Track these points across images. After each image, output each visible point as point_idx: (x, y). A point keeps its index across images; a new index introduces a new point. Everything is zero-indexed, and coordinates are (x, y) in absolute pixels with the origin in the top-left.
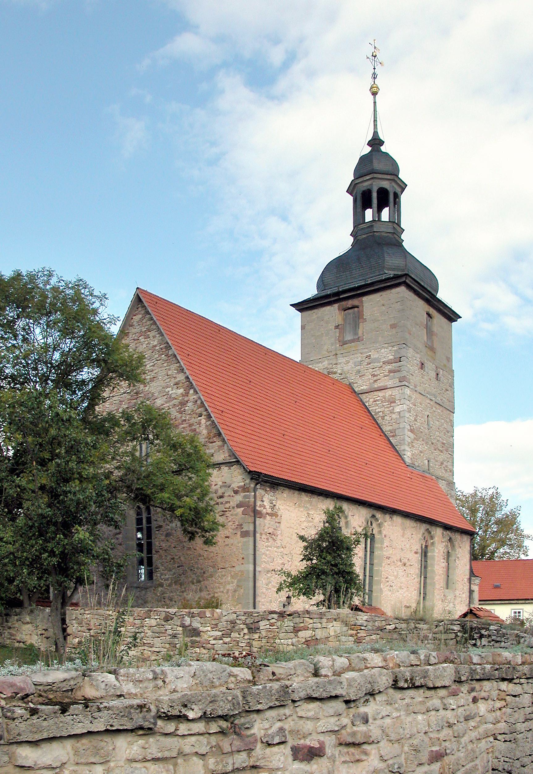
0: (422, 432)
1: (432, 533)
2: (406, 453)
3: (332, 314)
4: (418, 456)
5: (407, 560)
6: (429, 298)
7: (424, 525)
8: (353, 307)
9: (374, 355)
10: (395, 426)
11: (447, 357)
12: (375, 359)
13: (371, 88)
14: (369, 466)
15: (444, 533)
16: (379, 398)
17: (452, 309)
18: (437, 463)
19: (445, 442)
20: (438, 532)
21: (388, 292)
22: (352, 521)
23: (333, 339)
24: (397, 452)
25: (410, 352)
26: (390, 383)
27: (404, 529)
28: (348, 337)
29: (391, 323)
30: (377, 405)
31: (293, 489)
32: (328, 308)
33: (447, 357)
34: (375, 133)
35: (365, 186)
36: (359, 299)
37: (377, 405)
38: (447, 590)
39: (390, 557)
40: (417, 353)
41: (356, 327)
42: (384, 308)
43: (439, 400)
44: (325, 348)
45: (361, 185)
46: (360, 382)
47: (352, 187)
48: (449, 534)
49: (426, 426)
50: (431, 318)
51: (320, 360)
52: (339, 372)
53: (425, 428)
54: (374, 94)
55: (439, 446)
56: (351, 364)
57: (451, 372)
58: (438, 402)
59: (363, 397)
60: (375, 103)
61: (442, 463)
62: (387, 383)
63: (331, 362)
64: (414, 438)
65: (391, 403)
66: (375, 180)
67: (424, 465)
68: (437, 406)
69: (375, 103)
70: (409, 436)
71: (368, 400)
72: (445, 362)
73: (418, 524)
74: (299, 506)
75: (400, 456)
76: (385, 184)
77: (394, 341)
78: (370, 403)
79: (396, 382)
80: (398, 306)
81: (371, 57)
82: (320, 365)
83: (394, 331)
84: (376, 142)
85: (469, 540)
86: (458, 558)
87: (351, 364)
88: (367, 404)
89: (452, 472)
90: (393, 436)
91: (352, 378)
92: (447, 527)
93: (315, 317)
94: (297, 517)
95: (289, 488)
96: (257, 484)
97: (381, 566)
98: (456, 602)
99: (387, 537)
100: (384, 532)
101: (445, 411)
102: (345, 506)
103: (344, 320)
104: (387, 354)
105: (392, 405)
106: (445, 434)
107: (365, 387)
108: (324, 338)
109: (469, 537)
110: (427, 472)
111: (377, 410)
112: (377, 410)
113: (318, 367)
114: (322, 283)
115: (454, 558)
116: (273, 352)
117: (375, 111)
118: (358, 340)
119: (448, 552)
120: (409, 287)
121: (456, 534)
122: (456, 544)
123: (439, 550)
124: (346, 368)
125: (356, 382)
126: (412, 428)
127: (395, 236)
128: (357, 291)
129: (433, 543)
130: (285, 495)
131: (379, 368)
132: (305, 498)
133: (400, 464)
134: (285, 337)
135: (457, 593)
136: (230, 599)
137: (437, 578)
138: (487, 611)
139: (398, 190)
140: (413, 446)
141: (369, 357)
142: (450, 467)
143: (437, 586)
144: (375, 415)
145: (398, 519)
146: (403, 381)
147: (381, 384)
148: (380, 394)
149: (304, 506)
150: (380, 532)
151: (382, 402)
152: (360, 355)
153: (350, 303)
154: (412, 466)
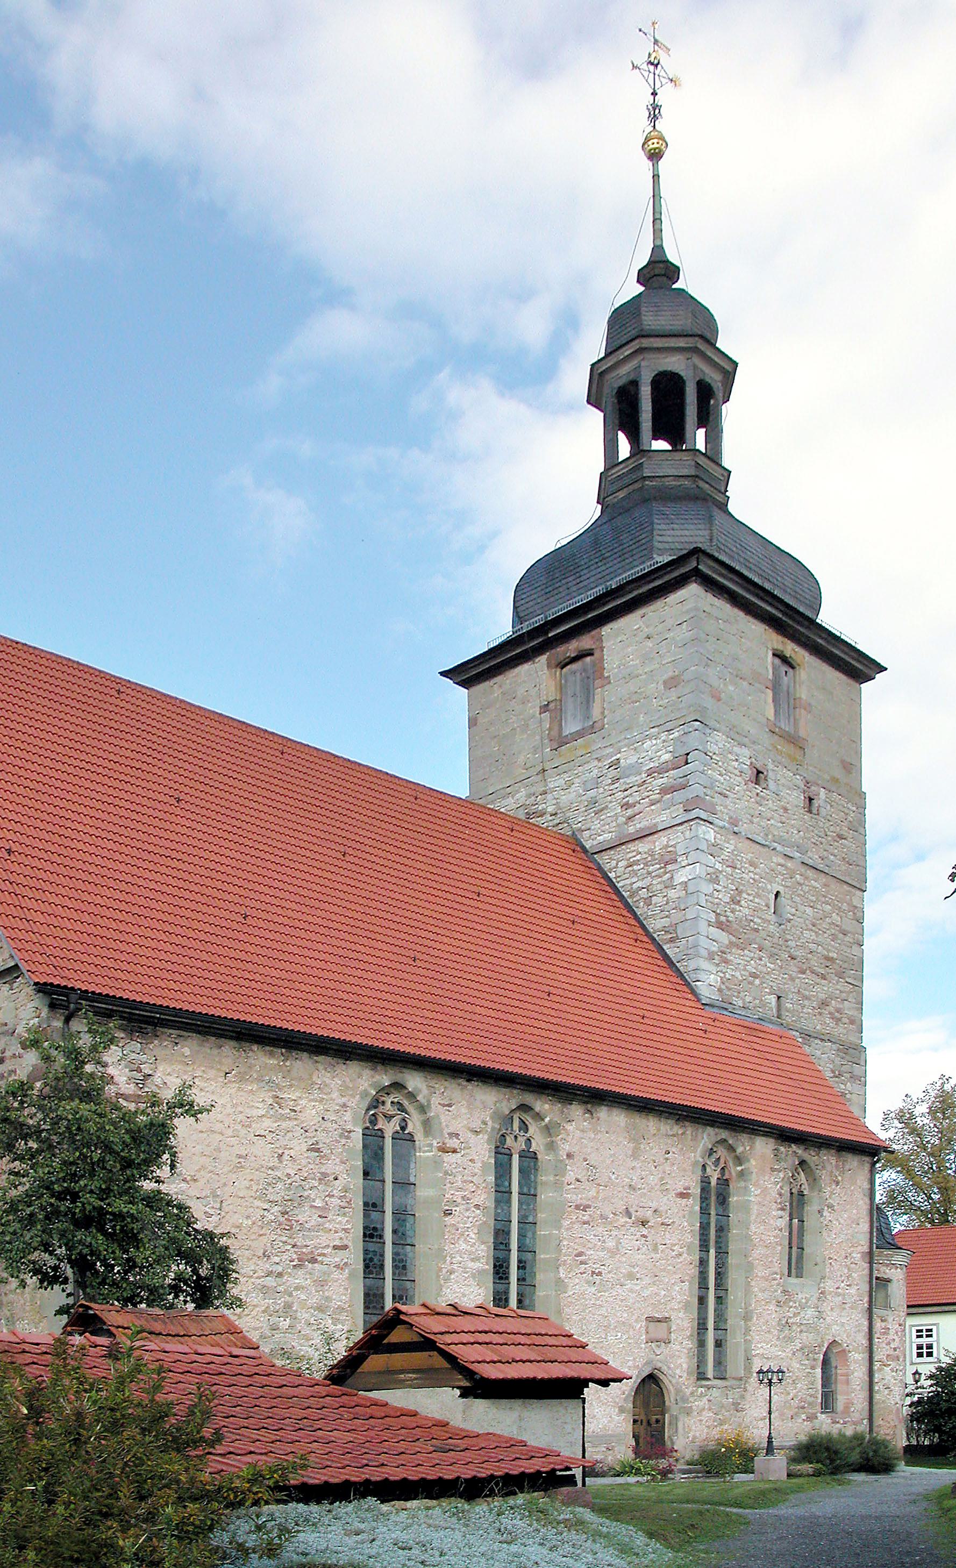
0: (757, 930)
1: (740, 1150)
2: (702, 976)
3: (535, 678)
4: (744, 984)
5: (650, 1213)
6: (774, 611)
7: (709, 1130)
10: (676, 916)
11: (843, 762)
12: (631, 766)
13: (647, 140)
14: (558, 999)
15: (782, 1149)
16: (638, 857)
17: (858, 647)
18: (806, 1003)
20: (761, 1149)
21: (659, 604)
22: (443, 1119)
23: (538, 737)
24: (681, 975)
25: (718, 742)
26: (663, 818)
27: (637, 1139)
28: (571, 727)
29: (665, 677)
30: (635, 873)
31: (214, 1035)
32: (524, 669)
33: (843, 762)
34: (658, 249)
35: (623, 373)
36: (593, 633)
37: (635, 873)
38: (793, 1280)
39: (589, 1207)
40: (741, 744)
41: (588, 702)
42: (649, 644)
43: (813, 857)
44: (521, 759)
45: (614, 374)
46: (596, 825)
47: (594, 386)
48: (800, 1152)
49: (773, 918)
50: (793, 667)
52: (550, 809)
54: (655, 156)
55: (813, 963)
56: (577, 788)
57: (859, 798)
58: (810, 862)
59: (603, 859)
60: (656, 177)
62: (657, 820)
63: (533, 790)
64: (731, 943)
65: (667, 863)
66: (646, 355)
67: (763, 1005)
68: (810, 873)
69: (656, 177)
70: (709, 937)
71: (614, 864)
72: (838, 773)
73: (690, 1129)
74: (242, 1078)
75: (687, 984)
76: (675, 363)
77: (673, 716)
78: (620, 870)
79: (678, 814)
80: (683, 633)
81: (645, 66)
82: (510, 800)
83: (673, 694)
84: (659, 273)
85: (867, 1167)
86: (830, 1206)
87: (577, 788)
88: (612, 875)
90: (672, 940)
91: (578, 820)
92: (786, 1136)
93: (497, 692)
94: (234, 1106)
95: (199, 1033)
96: (67, 1020)
97: (559, 1228)
98: (826, 1307)
99: (578, 1158)
100: (564, 1148)
101: (834, 885)
102: (415, 1081)
103: (561, 688)
104: (658, 750)
105: (669, 867)
106: (834, 937)
107: (607, 836)
108: (518, 738)
109: (867, 1159)
110: (771, 1022)
111: (635, 886)
112: (635, 886)
113: (507, 805)
114: (518, 617)
115: (816, 1207)
116: (386, 777)
117: (656, 196)
118: (592, 729)
119: (801, 1194)
120: (709, 584)
121: (823, 1152)
122: (824, 1175)
123: (765, 1191)
124: (565, 799)
125: (588, 826)
126: (723, 919)
127: (701, 484)
128: (586, 613)
129: (741, 1174)
130: (187, 1051)
131: (639, 786)
132: (262, 1059)
133: (688, 1003)
134: (429, 743)
135: (829, 1285)
136: (27, 1308)
137: (757, 1253)
138: (376, 1403)
139: (714, 377)
140: (726, 962)
143: (760, 1271)
144: (631, 896)
145: (614, 1120)
146: (697, 811)
148: (642, 846)
149: (259, 1080)
150: (551, 1147)
151: (646, 864)
152: (596, 763)
153: (573, 647)
154: (725, 1006)
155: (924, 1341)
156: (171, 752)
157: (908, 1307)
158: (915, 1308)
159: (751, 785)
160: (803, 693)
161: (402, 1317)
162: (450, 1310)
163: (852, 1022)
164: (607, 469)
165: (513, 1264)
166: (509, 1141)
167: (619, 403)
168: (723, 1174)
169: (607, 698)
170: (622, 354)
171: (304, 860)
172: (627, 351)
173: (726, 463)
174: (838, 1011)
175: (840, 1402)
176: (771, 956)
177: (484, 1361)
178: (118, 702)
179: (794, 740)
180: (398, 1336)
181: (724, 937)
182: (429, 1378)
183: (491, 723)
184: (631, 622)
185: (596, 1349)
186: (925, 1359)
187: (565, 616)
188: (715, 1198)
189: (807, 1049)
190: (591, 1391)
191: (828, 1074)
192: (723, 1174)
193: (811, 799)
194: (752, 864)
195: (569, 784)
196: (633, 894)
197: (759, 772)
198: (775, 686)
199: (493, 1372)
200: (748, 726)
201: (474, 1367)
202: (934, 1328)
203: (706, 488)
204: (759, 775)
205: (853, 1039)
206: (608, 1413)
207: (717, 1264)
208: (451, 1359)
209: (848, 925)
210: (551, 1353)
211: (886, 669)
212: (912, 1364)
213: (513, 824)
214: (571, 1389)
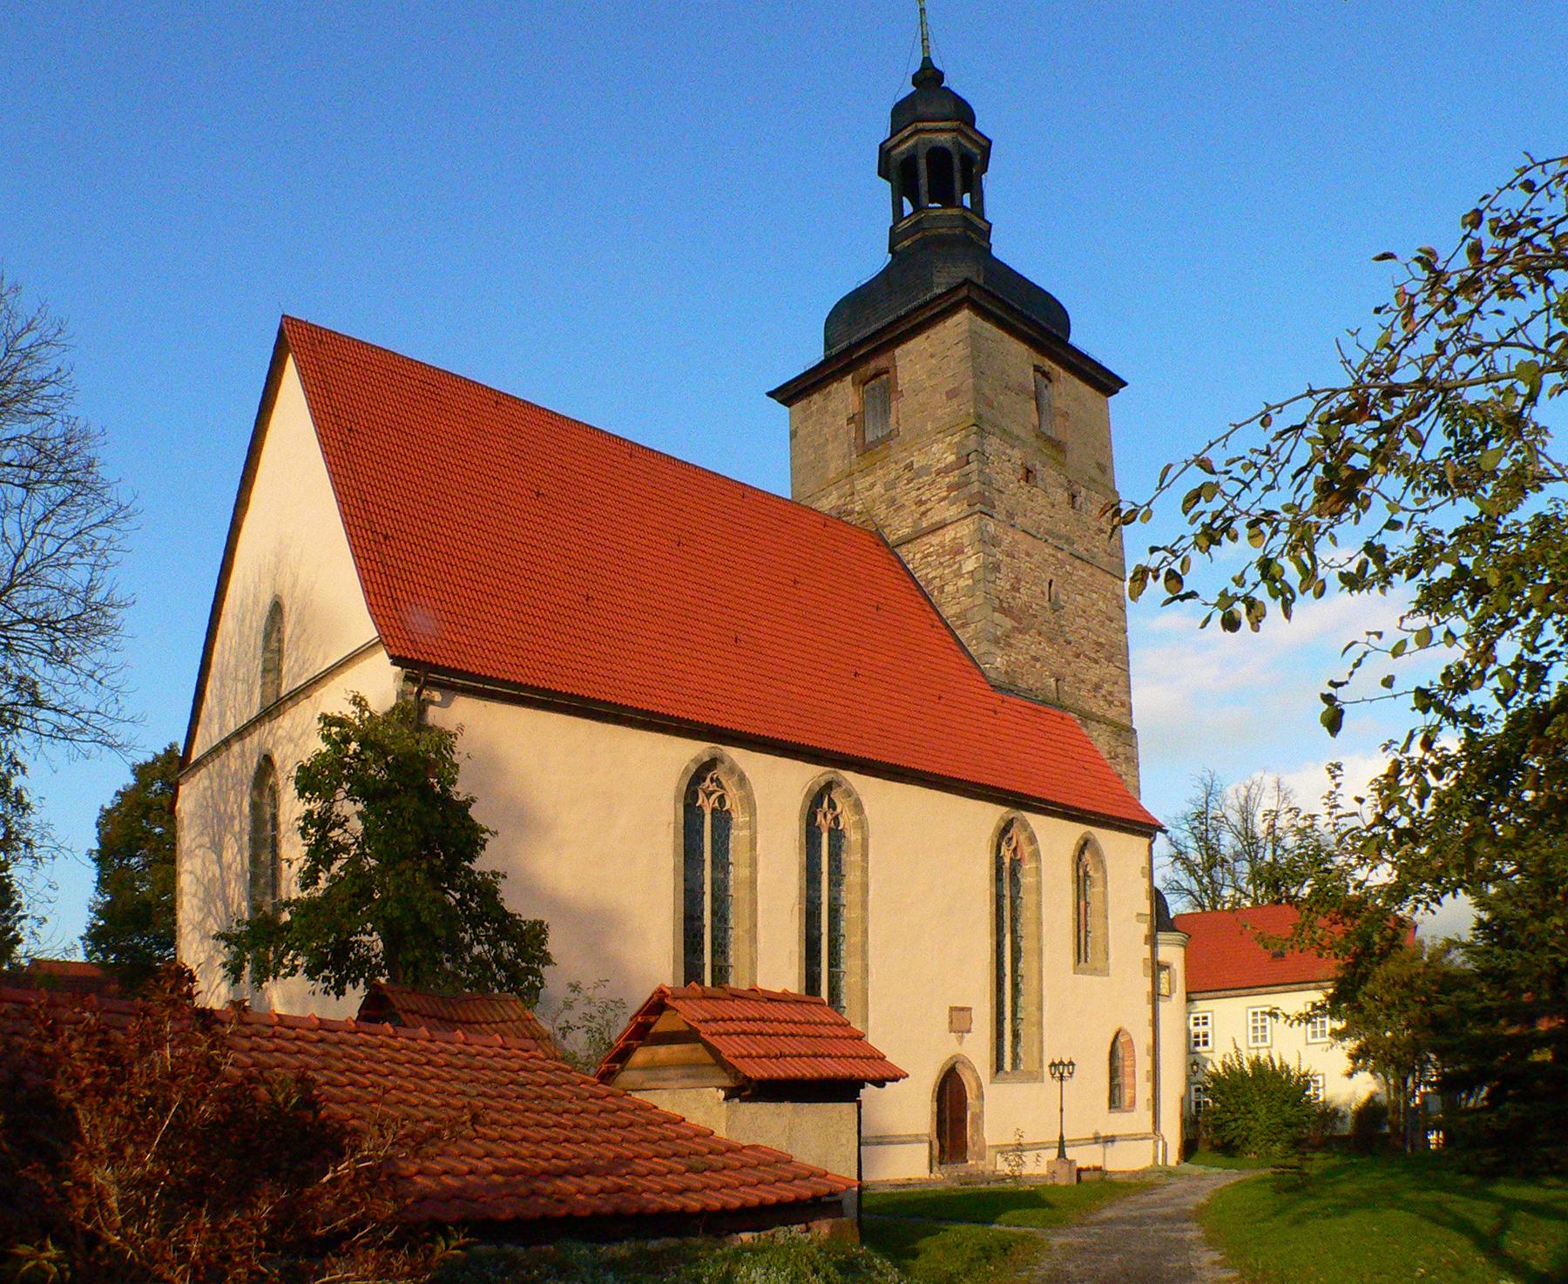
3: (844, 395)
8: (876, 376)
9: (919, 461)
19: (1102, 640)
26: (952, 512)
40: (1013, 447)
46: (896, 522)
49: (1046, 604)
51: (823, 491)
53: (1043, 607)
56: (879, 489)
61: (1097, 687)
68: (1078, 562)
72: (1094, 473)
78: (917, 563)
87: (879, 489)
88: (910, 566)
89: (1127, 707)
101: (1098, 573)
103: (864, 403)
113: (827, 504)
114: (828, 344)
134: (755, 449)
140: (1010, 645)
141: (909, 467)
142: (1124, 698)
147: (937, 518)
148: (934, 539)
153: (872, 366)
159: (1022, 483)
160: (1059, 403)
163: (1123, 705)
164: (896, 223)
165: (823, 936)
167: (898, 170)
169: (903, 410)
170: (900, 136)
172: (906, 133)
173: (987, 217)
174: (1111, 693)
176: (1050, 640)
179: (1058, 446)
180: (663, 1024)
181: (1009, 623)
182: (691, 1071)
183: (809, 434)
184: (918, 344)
187: (863, 339)
188: (1007, 877)
189: (1084, 731)
190: (868, 1092)
191: (1105, 756)
193: (1074, 497)
194: (1028, 554)
195: (873, 485)
196: (929, 582)
197: (1029, 471)
198: (1037, 397)
200: (1016, 430)
203: (975, 234)
205: (1125, 721)
206: (906, 1108)
207: (830, 941)
209: (1115, 613)
213: (826, 520)
214: (844, 1090)
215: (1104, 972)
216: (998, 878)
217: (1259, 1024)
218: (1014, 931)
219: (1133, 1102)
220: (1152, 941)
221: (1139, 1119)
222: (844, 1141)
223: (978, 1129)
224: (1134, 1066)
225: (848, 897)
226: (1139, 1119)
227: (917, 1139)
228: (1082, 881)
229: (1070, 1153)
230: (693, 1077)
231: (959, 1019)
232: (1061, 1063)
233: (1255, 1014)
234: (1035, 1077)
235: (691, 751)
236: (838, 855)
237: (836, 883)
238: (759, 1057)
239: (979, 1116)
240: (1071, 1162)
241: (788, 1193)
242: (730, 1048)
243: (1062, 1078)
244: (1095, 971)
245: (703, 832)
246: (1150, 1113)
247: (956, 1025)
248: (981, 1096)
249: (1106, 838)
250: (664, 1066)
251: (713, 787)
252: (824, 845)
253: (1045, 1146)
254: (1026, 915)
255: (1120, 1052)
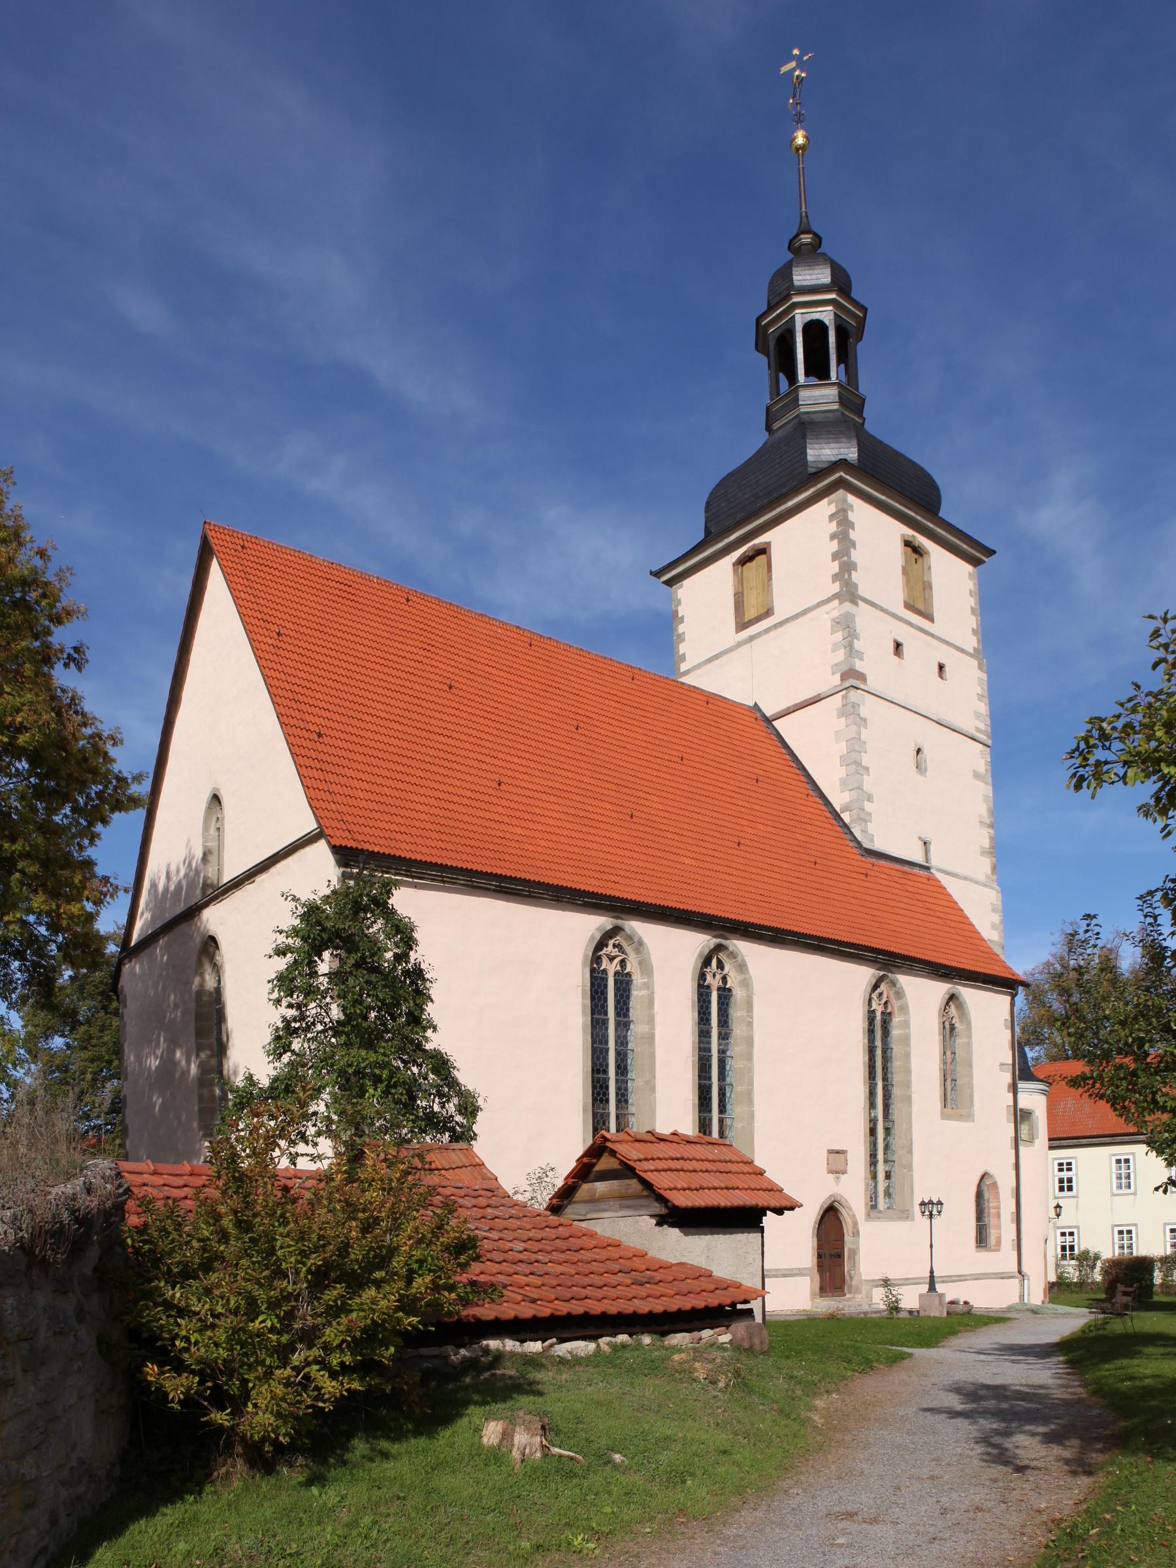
155: (1065, 1175)
156: (445, 647)
157: (1050, 1140)
158: (1056, 1142)
161: (609, 1144)
162: (650, 1137)
165: (713, 1087)
166: (709, 978)
168: (886, 1008)
171: (423, 800)
175: (992, 1234)
177: (675, 1189)
178: (406, 608)
182: (624, 1201)
185: (774, 1175)
186: (1066, 1193)
188: (880, 1030)
190: (769, 1220)
192: (886, 1008)
199: (682, 1200)
201: (667, 1194)
202: (1073, 1162)
204: (898, 646)
206: (789, 1240)
208: (647, 1185)
210: (734, 1181)
211: (994, 552)
212: (1056, 1198)
214: (746, 1219)
215: (968, 1117)
216: (871, 1031)
217: (1126, 1242)
218: (885, 1079)
219: (999, 1242)
220: (1014, 1089)
221: (1005, 1259)
222: (751, 1261)
223: (854, 1265)
224: (998, 1208)
225: (735, 1050)
226: (1005, 1259)
227: (799, 1273)
228: (949, 1031)
229: (940, 1288)
230: (628, 1207)
231: (837, 1159)
232: (931, 1202)
233: (1121, 1232)
234: (906, 1215)
235: (593, 924)
236: (726, 1010)
237: (724, 1036)
238: (684, 1190)
239: (854, 1253)
240: (942, 1296)
241: (713, 1301)
242: (660, 1181)
243: (931, 1216)
244: (960, 1118)
245: (609, 998)
246: (1016, 1253)
247: (834, 1168)
248: (856, 1233)
249: (971, 995)
250: (603, 1198)
251: (615, 952)
252: (715, 1008)
253: (915, 1282)
254: (896, 1065)
255: (986, 1196)
